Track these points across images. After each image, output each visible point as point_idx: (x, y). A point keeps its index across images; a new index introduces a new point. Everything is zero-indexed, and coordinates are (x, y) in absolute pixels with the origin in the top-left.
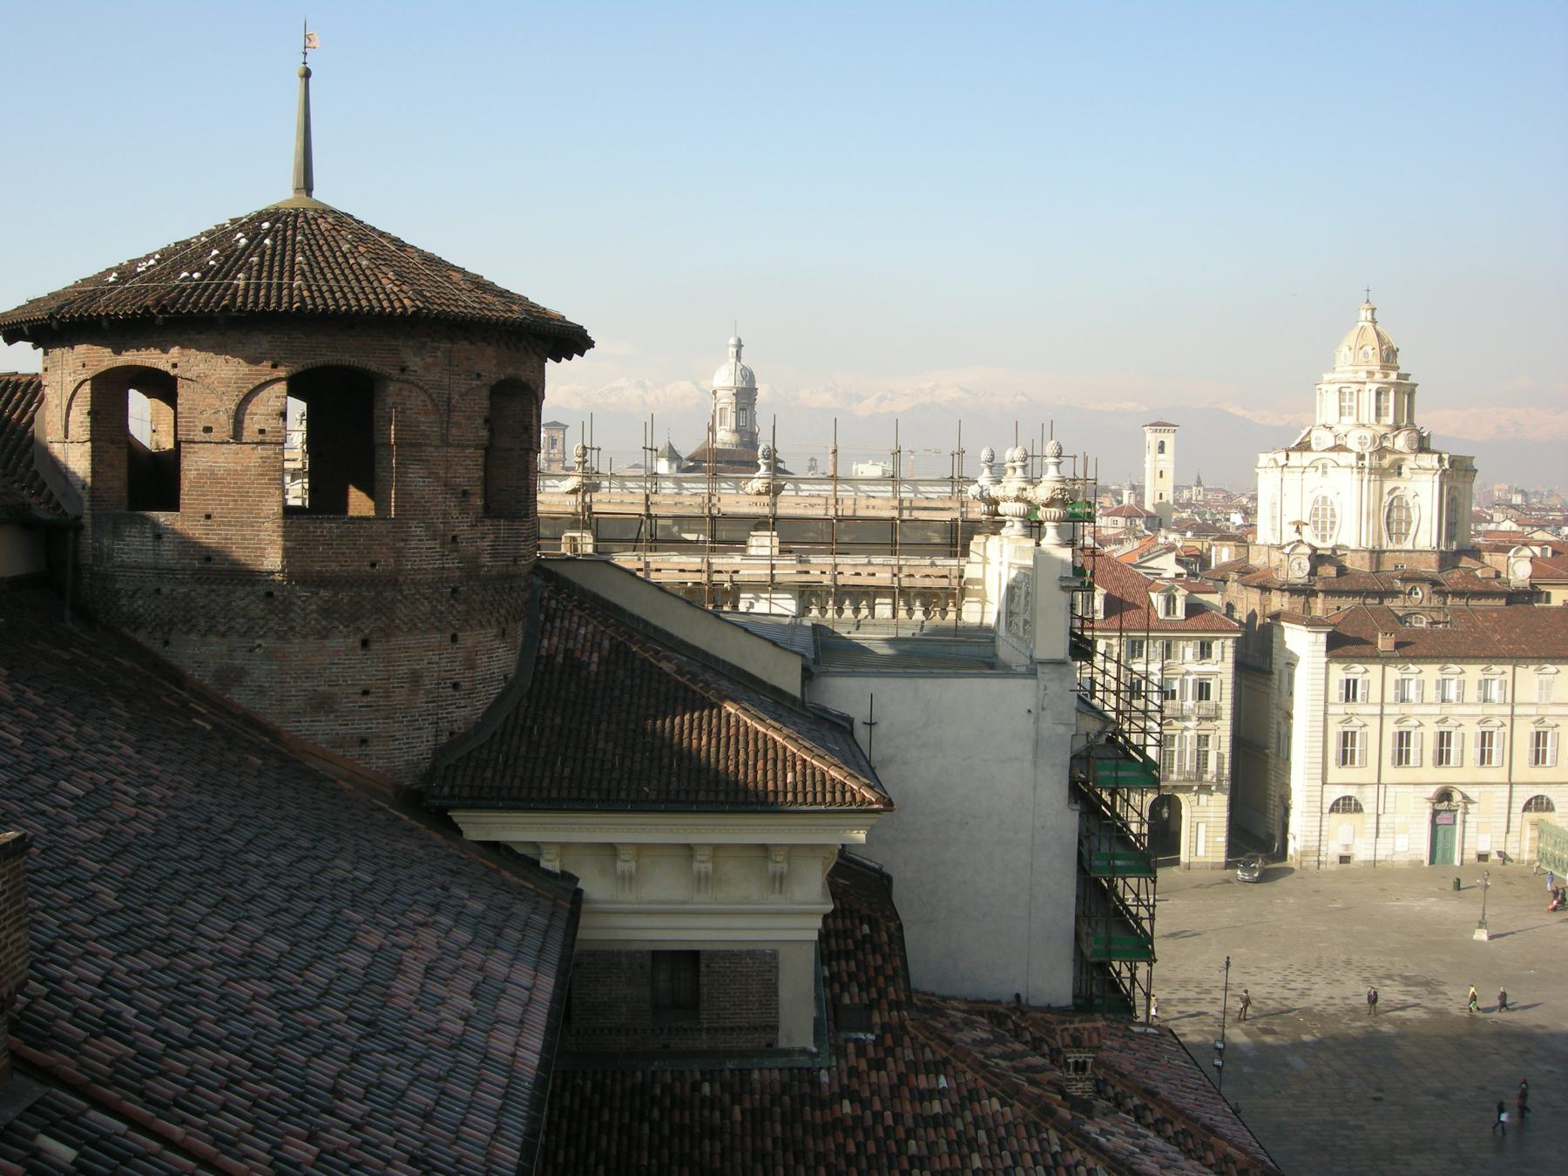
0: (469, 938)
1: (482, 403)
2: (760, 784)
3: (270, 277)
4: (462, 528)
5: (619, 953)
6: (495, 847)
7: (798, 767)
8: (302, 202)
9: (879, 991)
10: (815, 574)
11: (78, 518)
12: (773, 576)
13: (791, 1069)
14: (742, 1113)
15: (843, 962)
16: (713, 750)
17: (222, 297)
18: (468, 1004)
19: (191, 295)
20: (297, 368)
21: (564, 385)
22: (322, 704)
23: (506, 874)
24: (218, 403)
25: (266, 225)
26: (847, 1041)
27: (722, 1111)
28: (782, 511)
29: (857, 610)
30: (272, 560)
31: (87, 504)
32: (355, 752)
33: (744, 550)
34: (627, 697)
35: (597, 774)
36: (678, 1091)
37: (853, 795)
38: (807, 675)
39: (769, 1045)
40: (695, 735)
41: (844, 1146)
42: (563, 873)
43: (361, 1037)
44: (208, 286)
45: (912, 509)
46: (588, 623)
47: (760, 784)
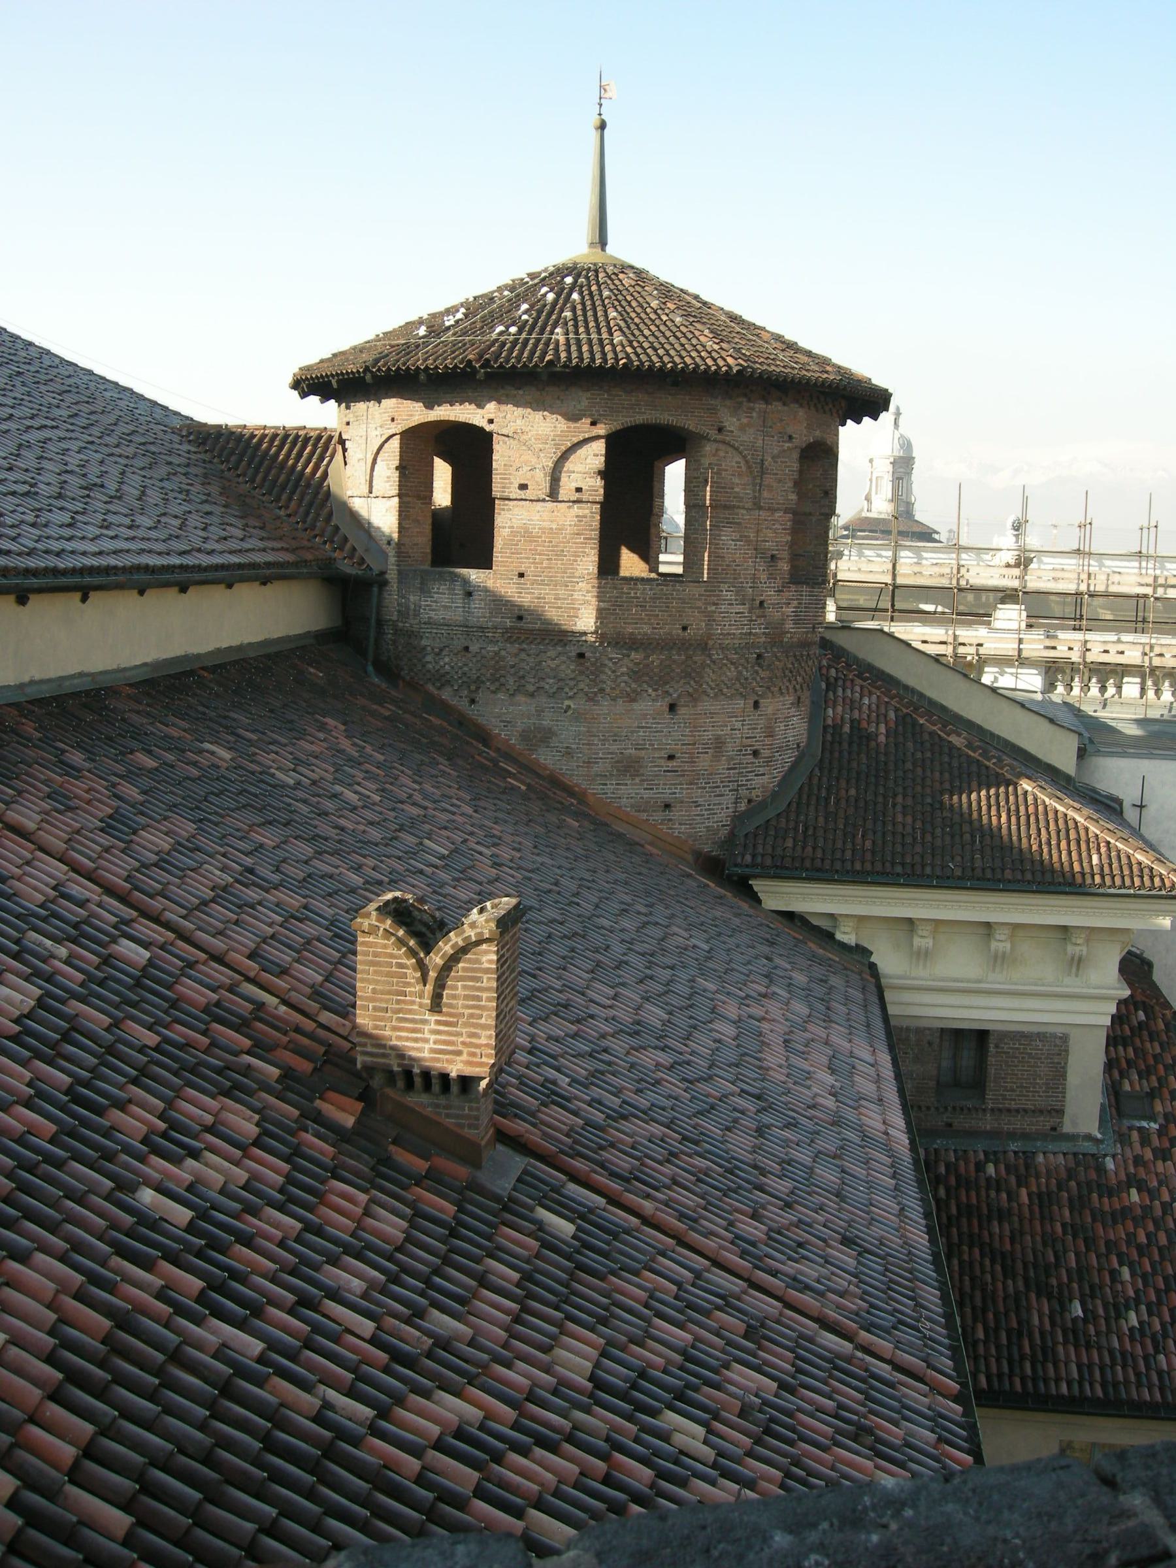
0: (806, 1011)
1: (792, 464)
2: (1066, 864)
3: (588, 332)
4: (770, 595)
5: (908, 1029)
6: (790, 916)
7: (1103, 850)
8: (597, 257)
9: (1159, 1080)
10: (1061, 652)
11: (383, 573)
12: (1020, 650)
13: (1075, 1154)
14: (1029, 1195)
15: (1121, 1048)
16: (1013, 827)
17: (544, 353)
18: (830, 1079)
19: (511, 350)
20: (616, 426)
21: (860, 446)
22: (629, 767)
23: (811, 945)
24: (534, 460)
25: (569, 280)
26: (1130, 1128)
27: (1009, 1194)
28: (1033, 584)
29: (1103, 689)
30: (586, 621)
31: (392, 560)
32: (659, 816)
33: (989, 623)
34: (919, 770)
35: (899, 848)
36: (962, 1170)
37: (1162, 880)
38: (1082, 753)
39: (1054, 1129)
40: (993, 812)
41: (1135, 1235)
42: (857, 945)
43: (758, 1111)
44: (526, 341)
45: (1166, 586)
46: (870, 693)
47: (1066, 864)
